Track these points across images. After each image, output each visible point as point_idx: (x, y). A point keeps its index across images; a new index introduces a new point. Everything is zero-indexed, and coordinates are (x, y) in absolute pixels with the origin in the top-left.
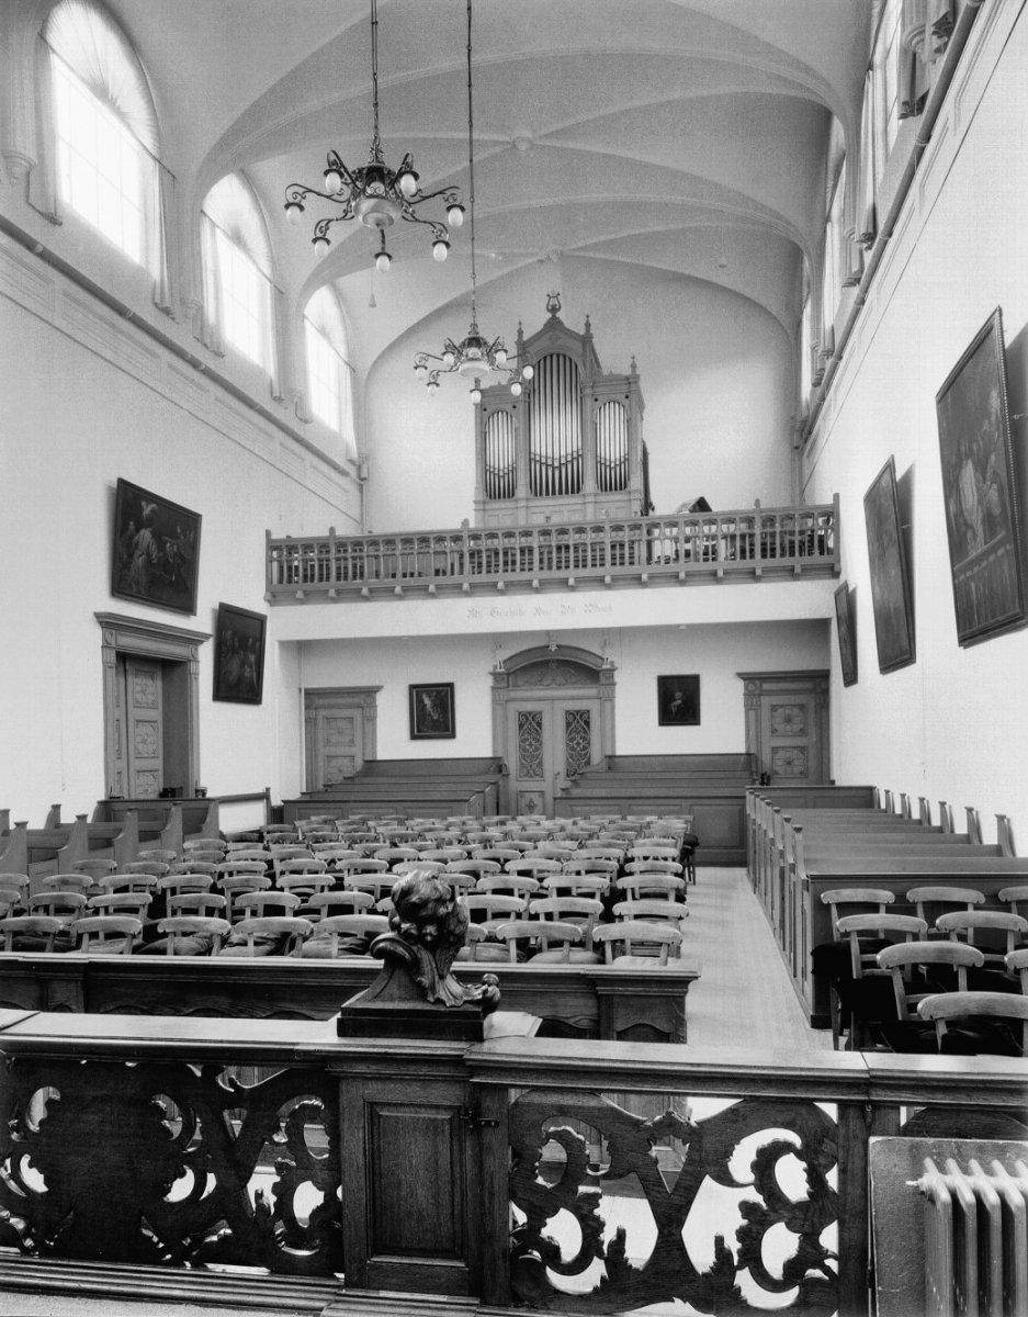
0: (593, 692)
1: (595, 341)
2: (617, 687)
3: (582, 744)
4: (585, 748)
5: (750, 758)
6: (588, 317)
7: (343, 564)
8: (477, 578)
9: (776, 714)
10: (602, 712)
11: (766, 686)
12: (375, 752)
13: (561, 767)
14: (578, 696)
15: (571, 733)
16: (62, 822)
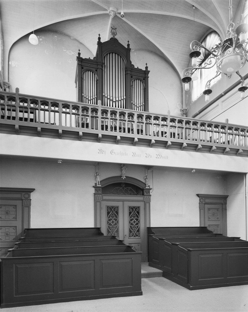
3: (115, 222)
4: (137, 224)
5: (202, 230)
9: (210, 212)
10: (145, 209)
13: (127, 232)
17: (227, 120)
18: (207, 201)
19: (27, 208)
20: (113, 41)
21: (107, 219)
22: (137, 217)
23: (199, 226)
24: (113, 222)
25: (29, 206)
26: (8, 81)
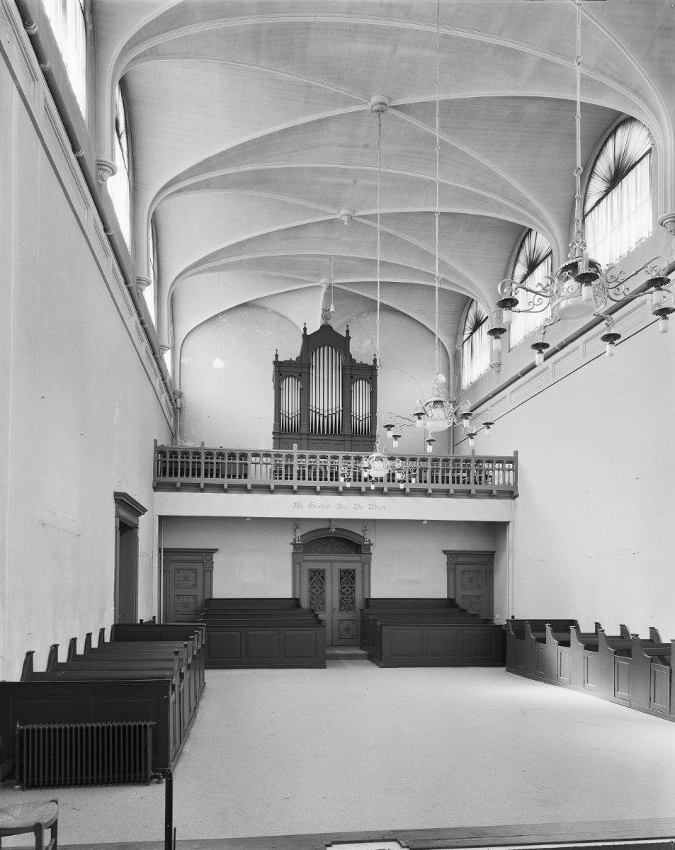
0: (357, 558)
1: (352, 343)
2: (373, 556)
4: (351, 593)
5: (450, 603)
7: (446, 475)
8: (302, 483)
9: (465, 576)
10: (363, 572)
11: (460, 559)
12: (370, 594)
13: (336, 604)
14: (348, 561)
15: (343, 584)
16: (619, 635)
17: (473, 451)
18: (460, 559)
19: (209, 573)
20: (326, 329)
21: (340, 586)
22: (352, 583)
23: (446, 597)
24: (317, 590)
25: (211, 571)
26: (112, 160)
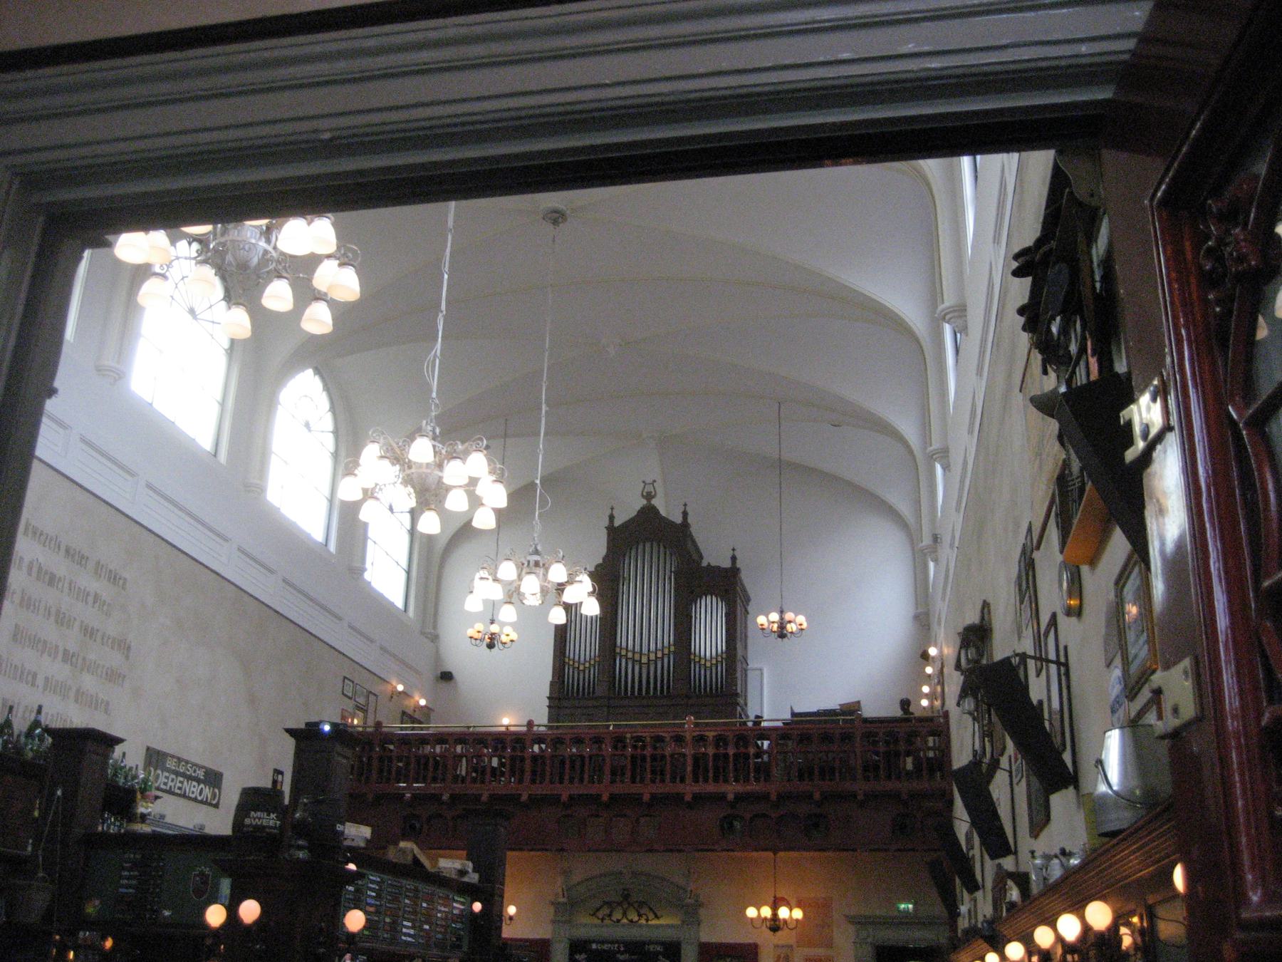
6: (612, 509)
